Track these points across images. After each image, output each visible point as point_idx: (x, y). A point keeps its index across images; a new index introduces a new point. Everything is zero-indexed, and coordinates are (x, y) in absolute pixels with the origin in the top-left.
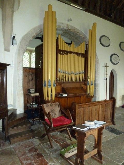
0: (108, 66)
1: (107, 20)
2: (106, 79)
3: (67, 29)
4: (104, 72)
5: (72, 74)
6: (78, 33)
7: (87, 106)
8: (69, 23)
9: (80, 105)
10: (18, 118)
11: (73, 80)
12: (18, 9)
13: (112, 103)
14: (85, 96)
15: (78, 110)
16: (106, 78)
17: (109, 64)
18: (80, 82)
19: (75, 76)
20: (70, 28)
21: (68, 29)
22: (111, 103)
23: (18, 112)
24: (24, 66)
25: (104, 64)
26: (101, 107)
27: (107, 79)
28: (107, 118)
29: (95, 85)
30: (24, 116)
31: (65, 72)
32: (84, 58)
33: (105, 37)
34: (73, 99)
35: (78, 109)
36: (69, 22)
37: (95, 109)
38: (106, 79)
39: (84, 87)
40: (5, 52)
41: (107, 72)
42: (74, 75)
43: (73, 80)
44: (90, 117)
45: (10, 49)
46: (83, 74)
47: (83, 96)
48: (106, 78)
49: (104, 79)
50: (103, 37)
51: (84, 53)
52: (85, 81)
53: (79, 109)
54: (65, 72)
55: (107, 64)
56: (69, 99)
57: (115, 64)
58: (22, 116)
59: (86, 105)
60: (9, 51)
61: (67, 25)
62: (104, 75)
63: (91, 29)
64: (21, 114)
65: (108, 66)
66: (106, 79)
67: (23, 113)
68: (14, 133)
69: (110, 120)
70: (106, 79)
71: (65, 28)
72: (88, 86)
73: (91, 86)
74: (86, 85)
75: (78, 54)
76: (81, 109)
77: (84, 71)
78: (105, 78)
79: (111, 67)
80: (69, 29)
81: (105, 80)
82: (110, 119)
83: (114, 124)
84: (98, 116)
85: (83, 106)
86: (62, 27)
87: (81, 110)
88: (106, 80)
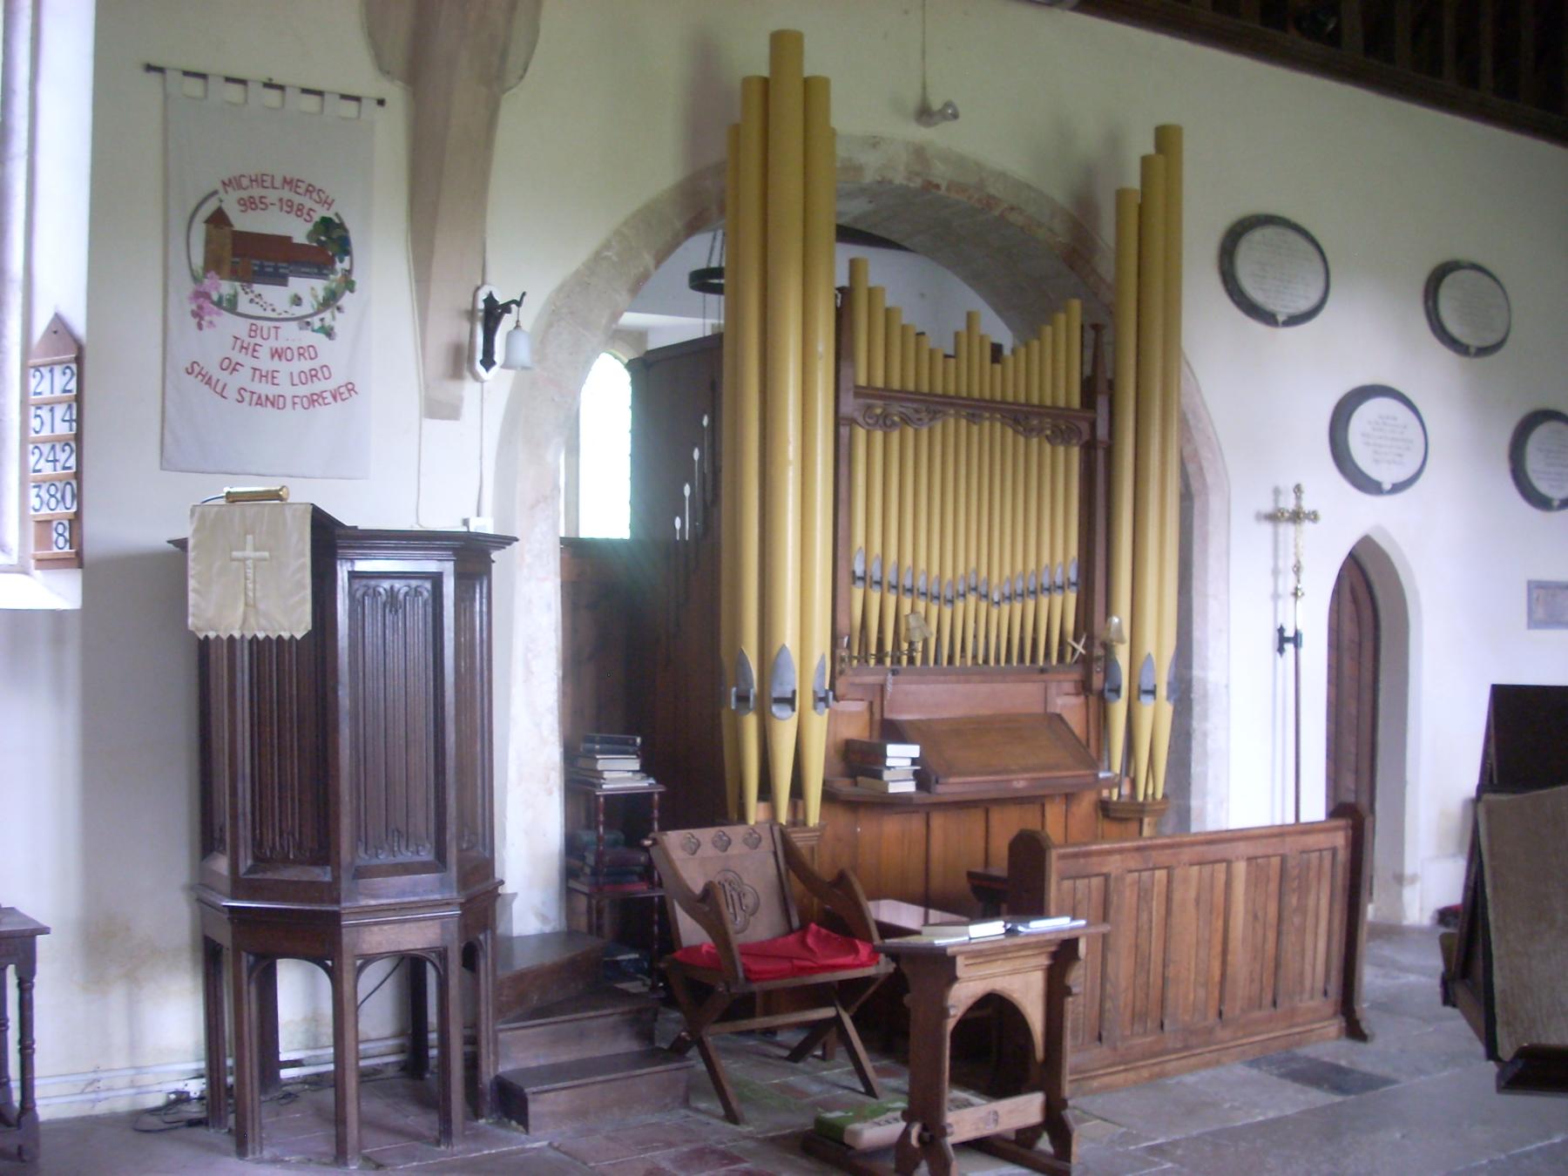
0: (1314, 517)
1: (1330, 666)
2: (1286, 640)
3: (917, 183)
4: (1276, 572)
5: (964, 595)
6: (1013, 217)
7: (1132, 864)
8: (935, 136)
9: (1076, 856)
10: (523, 961)
11: (975, 657)
12: (525, 70)
13: (1343, 856)
14: (1085, 805)
15: (1059, 890)
16: (1289, 633)
17: (1324, 487)
18: (1042, 671)
19: (994, 612)
20: (941, 172)
21: (930, 186)
22: (1334, 851)
23: (917, 755)
24: (587, 532)
25: (1277, 492)
26: (1247, 881)
27: (1296, 640)
28: (1302, 974)
29: (1183, 694)
30: (567, 955)
31: (891, 577)
32: (1075, 452)
33: (1268, 232)
34: (975, 820)
35: (1059, 884)
36: (928, 124)
37: (1192, 894)
38: (1286, 640)
39: (1075, 720)
40: (429, 424)
41: (1297, 569)
42: (983, 605)
43: (975, 657)
44: (1156, 958)
45: (461, 399)
46: (1072, 597)
47: (1069, 797)
48: (1289, 633)
49: (1270, 639)
50: (1257, 236)
51: (1076, 402)
52: (1091, 665)
53: (1067, 884)
54: (891, 577)
55: (1298, 489)
56: (937, 821)
57: (1387, 486)
58: (551, 957)
59: (1121, 851)
60: (1534, 623)
61: (919, 153)
62: (1276, 596)
63: (1134, 182)
64: (543, 938)
65: (1314, 517)
66: (1288, 640)
67: (554, 934)
68: (533, 1064)
69: (1318, 1001)
70: (1288, 640)
71: (899, 179)
72: (1119, 710)
73: (1147, 707)
74: (1096, 694)
75: (1021, 417)
76: (1081, 883)
77: (1073, 576)
78: (1281, 630)
79: (1344, 519)
80: (938, 187)
81: (1281, 650)
82: (1320, 985)
83: (1354, 1031)
84: (1218, 948)
85: (1094, 864)
86: (869, 177)
87: (1079, 896)
88: (1289, 647)
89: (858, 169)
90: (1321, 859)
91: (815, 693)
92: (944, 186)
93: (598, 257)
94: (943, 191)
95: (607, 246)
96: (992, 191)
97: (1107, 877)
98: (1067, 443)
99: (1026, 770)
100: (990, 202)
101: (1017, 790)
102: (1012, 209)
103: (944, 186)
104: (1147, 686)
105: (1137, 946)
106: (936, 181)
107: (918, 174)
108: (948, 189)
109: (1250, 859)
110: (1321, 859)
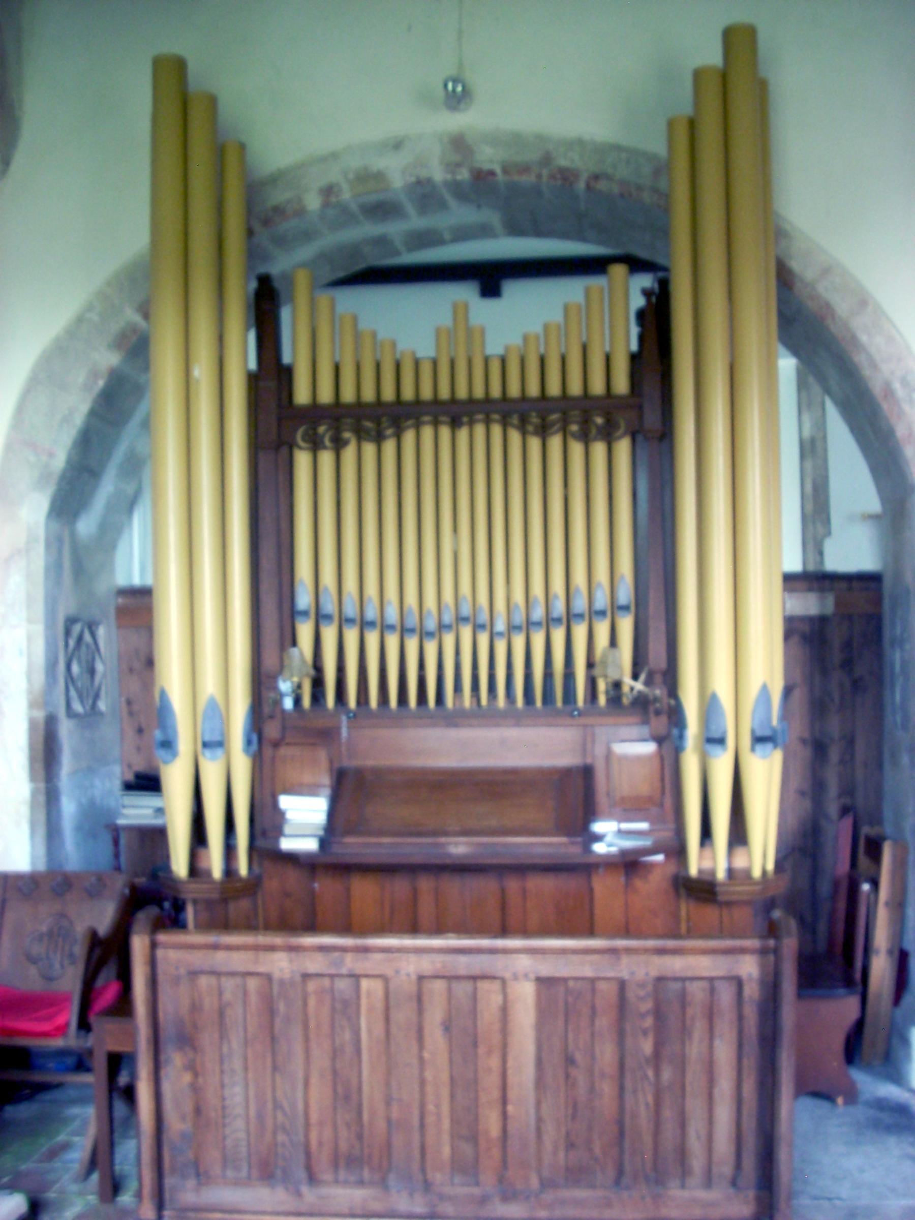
13: (752, 991)
20: (488, 157)
46: (626, 626)
61: (459, 144)
77: (625, 594)
80: (492, 173)
89: (380, 176)
90: (712, 991)
91: (753, 732)
92: (498, 171)
93: (80, 320)
94: (500, 177)
95: (89, 308)
96: (563, 162)
97: (268, 977)
98: (608, 435)
99: (466, 832)
100: (567, 176)
101: (450, 855)
102: (596, 177)
103: (498, 171)
104: (716, 735)
105: (335, 1072)
106: (486, 166)
107: (458, 165)
108: (505, 171)
109: (545, 983)
110: (712, 991)
